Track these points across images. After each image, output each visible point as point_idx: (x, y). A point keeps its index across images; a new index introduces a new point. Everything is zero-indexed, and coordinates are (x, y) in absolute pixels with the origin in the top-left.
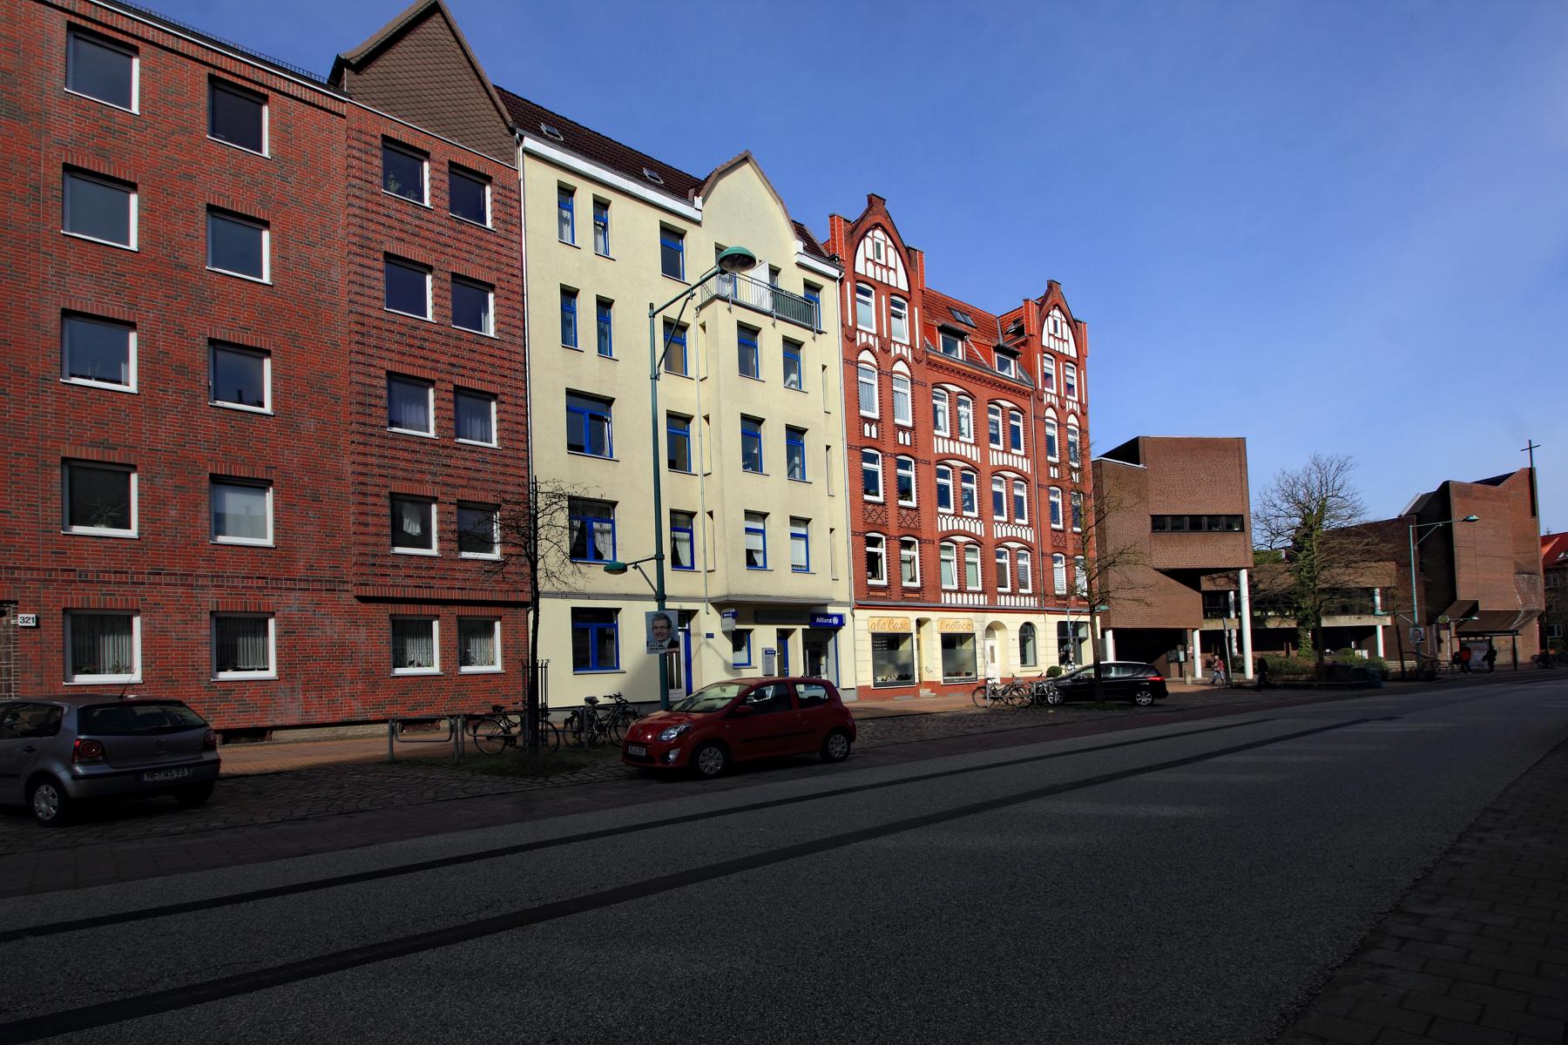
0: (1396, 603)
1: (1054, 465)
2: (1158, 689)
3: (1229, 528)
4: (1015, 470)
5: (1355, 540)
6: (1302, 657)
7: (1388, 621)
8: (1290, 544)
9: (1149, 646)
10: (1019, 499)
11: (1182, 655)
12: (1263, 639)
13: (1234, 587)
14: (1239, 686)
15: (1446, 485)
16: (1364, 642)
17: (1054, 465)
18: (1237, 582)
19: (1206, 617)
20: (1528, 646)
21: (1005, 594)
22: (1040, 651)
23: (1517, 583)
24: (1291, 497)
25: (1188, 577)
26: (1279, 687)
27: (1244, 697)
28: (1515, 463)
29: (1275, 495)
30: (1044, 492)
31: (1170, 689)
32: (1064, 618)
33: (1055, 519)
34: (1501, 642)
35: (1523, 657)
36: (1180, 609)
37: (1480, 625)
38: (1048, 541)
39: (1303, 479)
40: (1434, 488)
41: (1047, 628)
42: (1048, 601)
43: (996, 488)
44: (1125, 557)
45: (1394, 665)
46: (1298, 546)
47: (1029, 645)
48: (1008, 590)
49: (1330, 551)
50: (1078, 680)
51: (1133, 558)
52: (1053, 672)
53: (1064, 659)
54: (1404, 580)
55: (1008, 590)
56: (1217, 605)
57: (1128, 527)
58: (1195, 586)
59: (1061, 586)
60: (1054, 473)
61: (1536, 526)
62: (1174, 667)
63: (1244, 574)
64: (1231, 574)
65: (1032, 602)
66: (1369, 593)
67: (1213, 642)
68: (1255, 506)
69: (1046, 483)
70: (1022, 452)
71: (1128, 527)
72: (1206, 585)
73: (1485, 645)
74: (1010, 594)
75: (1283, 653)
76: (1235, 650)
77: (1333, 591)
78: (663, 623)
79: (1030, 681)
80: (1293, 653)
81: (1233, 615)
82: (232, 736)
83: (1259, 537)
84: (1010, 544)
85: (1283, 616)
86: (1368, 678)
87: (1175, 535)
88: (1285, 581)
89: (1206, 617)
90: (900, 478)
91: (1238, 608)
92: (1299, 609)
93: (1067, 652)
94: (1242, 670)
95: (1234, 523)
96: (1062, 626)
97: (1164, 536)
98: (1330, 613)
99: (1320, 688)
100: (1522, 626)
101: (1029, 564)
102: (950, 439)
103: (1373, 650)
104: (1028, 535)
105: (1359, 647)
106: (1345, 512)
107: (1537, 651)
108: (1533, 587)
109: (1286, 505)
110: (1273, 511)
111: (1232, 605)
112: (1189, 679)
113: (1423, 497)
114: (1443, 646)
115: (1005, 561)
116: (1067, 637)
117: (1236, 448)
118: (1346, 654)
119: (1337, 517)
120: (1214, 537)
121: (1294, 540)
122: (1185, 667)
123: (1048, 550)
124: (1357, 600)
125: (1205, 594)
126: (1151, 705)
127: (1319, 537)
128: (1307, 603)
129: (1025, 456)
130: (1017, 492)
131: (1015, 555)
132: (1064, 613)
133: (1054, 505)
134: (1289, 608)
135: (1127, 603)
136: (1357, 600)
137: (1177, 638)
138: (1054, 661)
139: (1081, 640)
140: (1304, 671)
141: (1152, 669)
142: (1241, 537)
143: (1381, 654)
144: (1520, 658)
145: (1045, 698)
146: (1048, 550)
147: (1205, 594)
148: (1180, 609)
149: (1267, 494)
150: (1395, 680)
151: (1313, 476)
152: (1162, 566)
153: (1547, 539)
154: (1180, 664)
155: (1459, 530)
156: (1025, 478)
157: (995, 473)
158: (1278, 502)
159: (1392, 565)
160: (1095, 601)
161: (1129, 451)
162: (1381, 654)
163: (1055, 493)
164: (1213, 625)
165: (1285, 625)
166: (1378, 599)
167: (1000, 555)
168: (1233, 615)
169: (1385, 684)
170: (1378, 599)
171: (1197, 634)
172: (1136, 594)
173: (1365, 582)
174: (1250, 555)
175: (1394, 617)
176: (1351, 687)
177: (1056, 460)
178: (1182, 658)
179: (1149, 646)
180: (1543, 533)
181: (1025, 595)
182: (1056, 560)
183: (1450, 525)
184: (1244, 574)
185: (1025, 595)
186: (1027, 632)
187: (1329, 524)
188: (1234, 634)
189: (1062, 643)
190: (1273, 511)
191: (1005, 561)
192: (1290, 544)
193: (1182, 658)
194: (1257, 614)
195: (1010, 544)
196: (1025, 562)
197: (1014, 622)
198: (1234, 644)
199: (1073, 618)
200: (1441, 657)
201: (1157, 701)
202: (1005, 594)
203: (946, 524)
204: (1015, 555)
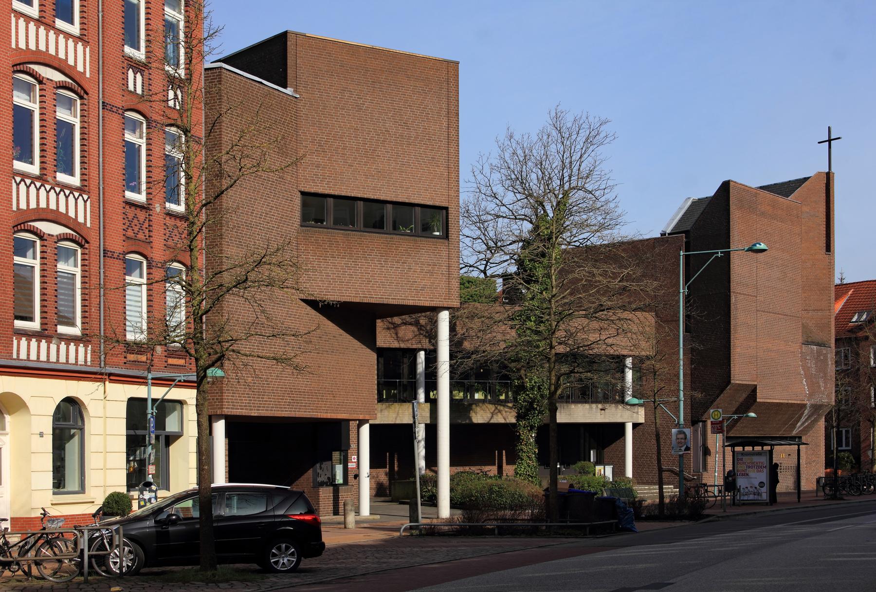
0: (658, 384)
1: (137, 67)
2: (307, 537)
3: (426, 229)
4: (59, 66)
5: (612, 268)
6: (520, 478)
7: (640, 416)
8: (513, 269)
9: (281, 450)
10: (171, 167)
11: (339, 470)
12: (472, 443)
13: (426, 343)
14: (432, 532)
15: (726, 186)
16: (608, 452)
17: (137, 67)
18: (433, 336)
19: (380, 400)
20: (807, 463)
21: (29, 335)
22: (92, 461)
23: (803, 359)
24: (519, 182)
25: (356, 319)
26: (489, 532)
27: (440, 553)
28: (808, 164)
29: (496, 176)
30: (114, 120)
31: (330, 538)
32: (140, 391)
33: (131, 180)
34: (783, 454)
35: (808, 484)
36: (338, 382)
37: (758, 428)
38: (117, 226)
39: (538, 152)
40: (710, 191)
41: (106, 409)
42: (113, 358)
43: (20, 99)
44: (264, 270)
45: (648, 493)
46: (526, 272)
47: (72, 447)
48: (35, 325)
49: (574, 287)
50: (169, 521)
51: (277, 272)
52: (115, 505)
53: (136, 478)
54: (665, 346)
55: (35, 325)
56: (398, 376)
57: (263, 214)
58: (367, 338)
59: (136, 330)
60: (135, 82)
61: (830, 267)
62: (326, 494)
63: (444, 318)
64: (422, 316)
65: (80, 356)
66: (619, 361)
67: (392, 444)
68: (466, 196)
69: (118, 101)
70: (75, 29)
71: (263, 214)
72: (384, 339)
73: (764, 460)
74: (39, 336)
75: (493, 470)
76: (421, 463)
77: (573, 357)
78: (682, 436)
79: (76, 523)
80: (509, 470)
81: (421, 396)
82: (711, 486)
83: (469, 250)
84: (45, 227)
85: (497, 402)
86: (611, 516)
87: (339, 235)
88: (501, 337)
89: (380, 400)
90: (17, 109)
91: (432, 384)
92: (522, 388)
93: (142, 463)
94: (432, 501)
95: (428, 221)
96: (135, 406)
97: (321, 235)
98: (569, 399)
99: (550, 533)
100: (806, 430)
101: (37, 264)
102: (39, 22)
103: (619, 470)
104: (80, 210)
105: (600, 461)
106: (596, 219)
107: (822, 472)
108: (821, 362)
109: (510, 197)
110: (491, 206)
111: (421, 379)
112: (351, 518)
113: (696, 204)
114: (710, 459)
115: (33, 261)
116: (145, 430)
117: (443, 76)
118: (584, 472)
119: (582, 225)
120: (402, 244)
121: (520, 263)
122: (343, 494)
123: (117, 244)
124: (593, 375)
125: (382, 353)
126: (295, 570)
127: (554, 261)
128: (533, 378)
129: (81, 38)
130: (63, 114)
131: (53, 251)
132: (139, 380)
133: (132, 151)
134: (506, 386)
135: (258, 364)
136: (593, 375)
137: (329, 437)
138: (118, 482)
139: (170, 439)
140: (518, 505)
141: (300, 497)
142: (442, 246)
143: (629, 473)
144: (804, 486)
145: (102, 561)
146: (117, 244)
147: (382, 353)
148: (338, 382)
149: (482, 171)
150: (650, 518)
151: (553, 148)
152: (335, 294)
153: (842, 289)
154: (336, 488)
155: (741, 267)
156: (77, 86)
157: (20, 67)
158: (499, 189)
159: (650, 318)
160: (204, 353)
161: (269, 58)
162: (629, 473)
163: (134, 126)
164: (396, 414)
165: (499, 419)
166: (629, 375)
167: (21, 248)
168: (421, 396)
169: (639, 526)
170: (629, 375)
171: (365, 430)
172: (277, 347)
173: (621, 345)
174: (455, 284)
175: (652, 409)
176: (595, 531)
177: (140, 55)
178: (339, 479)
179: (281, 450)
180: (837, 281)
181: (69, 339)
182: (130, 267)
183: (727, 255)
184: (444, 318)
185: (69, 339)
186: (69, 418)
187: (581, 235)
188: (421, 433)
189: (134, 443)
190: (491, 206)
191: (33, 261)
192: (513, 269)
193: (339, 479)
194: (459, 395)
195: (45, 227)
196: (70, 267)
197: (43, 396)
198: (420, 451)
199: (158, 392)
200: (707, 479)
201: (306, 563)
202: (29, 335)
203: (25, 197)
204: (53, 251)
